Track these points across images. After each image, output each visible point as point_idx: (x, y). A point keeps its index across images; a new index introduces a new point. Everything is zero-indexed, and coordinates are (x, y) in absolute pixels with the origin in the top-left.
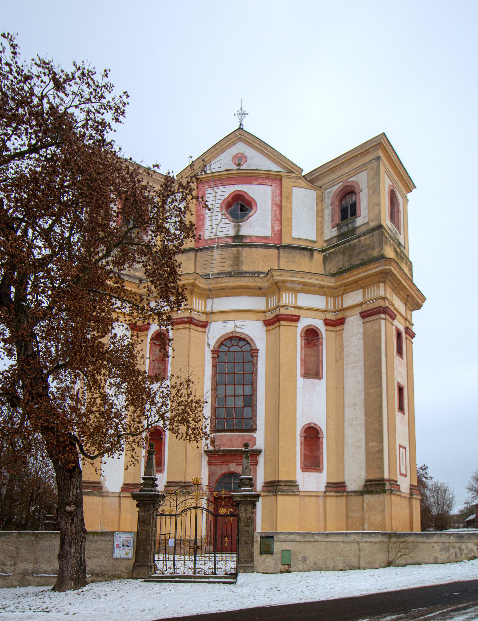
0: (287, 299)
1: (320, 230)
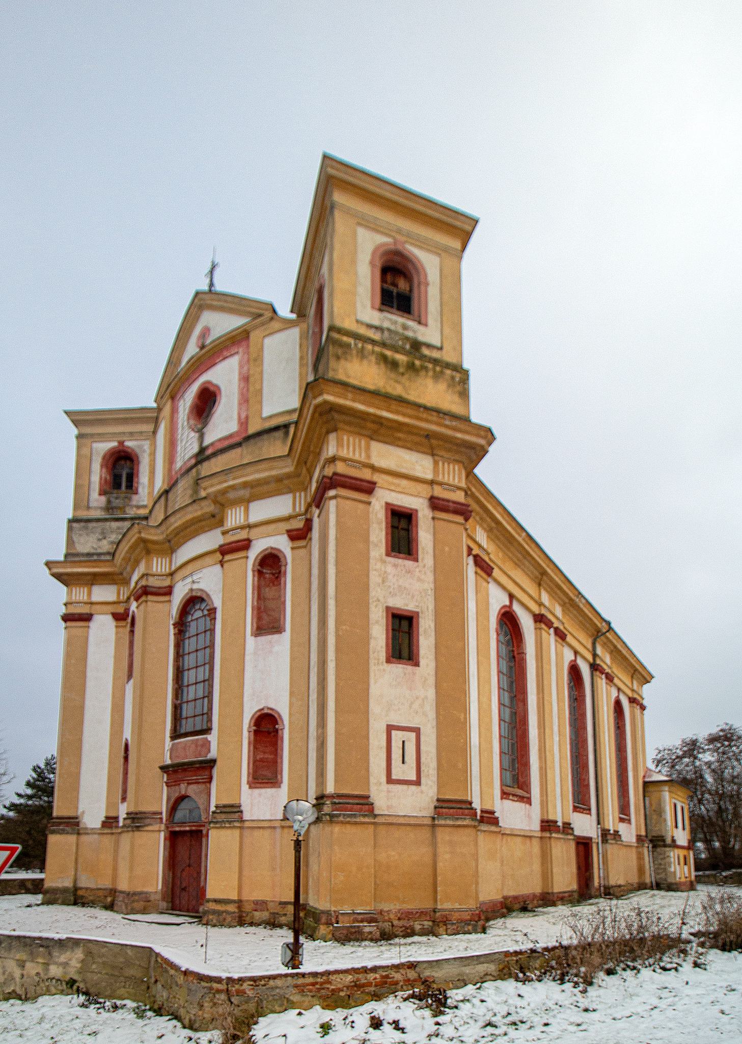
0: (234, 517)
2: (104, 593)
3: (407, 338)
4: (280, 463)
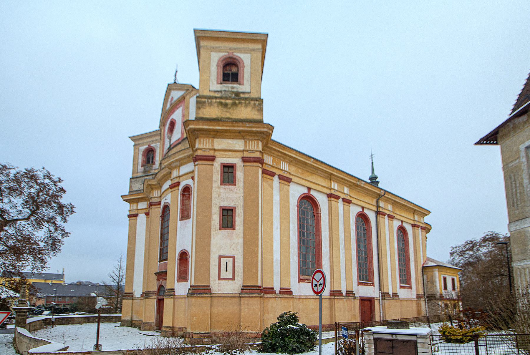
0: (175, 173)
2: (143, 205)
3: (233, 92)
4: (187, 151)
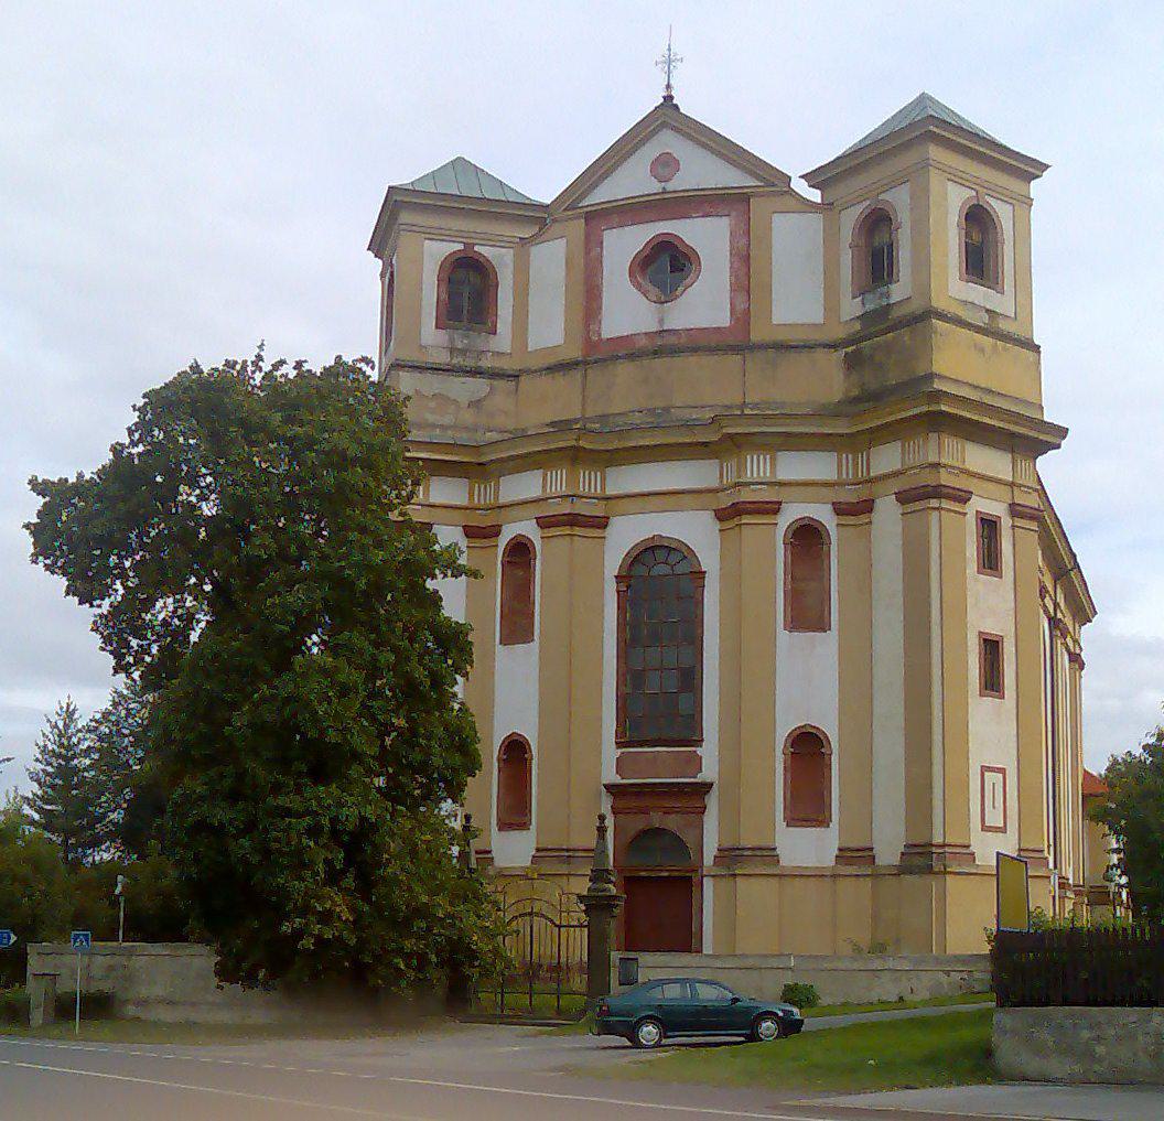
0: (757, 467)
1: (831, 306)
